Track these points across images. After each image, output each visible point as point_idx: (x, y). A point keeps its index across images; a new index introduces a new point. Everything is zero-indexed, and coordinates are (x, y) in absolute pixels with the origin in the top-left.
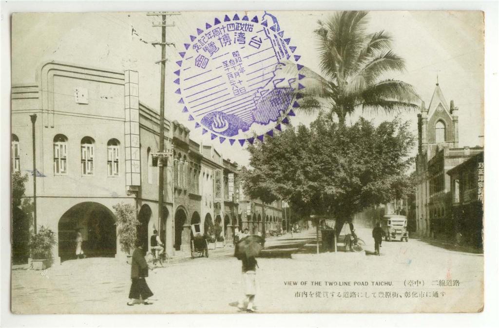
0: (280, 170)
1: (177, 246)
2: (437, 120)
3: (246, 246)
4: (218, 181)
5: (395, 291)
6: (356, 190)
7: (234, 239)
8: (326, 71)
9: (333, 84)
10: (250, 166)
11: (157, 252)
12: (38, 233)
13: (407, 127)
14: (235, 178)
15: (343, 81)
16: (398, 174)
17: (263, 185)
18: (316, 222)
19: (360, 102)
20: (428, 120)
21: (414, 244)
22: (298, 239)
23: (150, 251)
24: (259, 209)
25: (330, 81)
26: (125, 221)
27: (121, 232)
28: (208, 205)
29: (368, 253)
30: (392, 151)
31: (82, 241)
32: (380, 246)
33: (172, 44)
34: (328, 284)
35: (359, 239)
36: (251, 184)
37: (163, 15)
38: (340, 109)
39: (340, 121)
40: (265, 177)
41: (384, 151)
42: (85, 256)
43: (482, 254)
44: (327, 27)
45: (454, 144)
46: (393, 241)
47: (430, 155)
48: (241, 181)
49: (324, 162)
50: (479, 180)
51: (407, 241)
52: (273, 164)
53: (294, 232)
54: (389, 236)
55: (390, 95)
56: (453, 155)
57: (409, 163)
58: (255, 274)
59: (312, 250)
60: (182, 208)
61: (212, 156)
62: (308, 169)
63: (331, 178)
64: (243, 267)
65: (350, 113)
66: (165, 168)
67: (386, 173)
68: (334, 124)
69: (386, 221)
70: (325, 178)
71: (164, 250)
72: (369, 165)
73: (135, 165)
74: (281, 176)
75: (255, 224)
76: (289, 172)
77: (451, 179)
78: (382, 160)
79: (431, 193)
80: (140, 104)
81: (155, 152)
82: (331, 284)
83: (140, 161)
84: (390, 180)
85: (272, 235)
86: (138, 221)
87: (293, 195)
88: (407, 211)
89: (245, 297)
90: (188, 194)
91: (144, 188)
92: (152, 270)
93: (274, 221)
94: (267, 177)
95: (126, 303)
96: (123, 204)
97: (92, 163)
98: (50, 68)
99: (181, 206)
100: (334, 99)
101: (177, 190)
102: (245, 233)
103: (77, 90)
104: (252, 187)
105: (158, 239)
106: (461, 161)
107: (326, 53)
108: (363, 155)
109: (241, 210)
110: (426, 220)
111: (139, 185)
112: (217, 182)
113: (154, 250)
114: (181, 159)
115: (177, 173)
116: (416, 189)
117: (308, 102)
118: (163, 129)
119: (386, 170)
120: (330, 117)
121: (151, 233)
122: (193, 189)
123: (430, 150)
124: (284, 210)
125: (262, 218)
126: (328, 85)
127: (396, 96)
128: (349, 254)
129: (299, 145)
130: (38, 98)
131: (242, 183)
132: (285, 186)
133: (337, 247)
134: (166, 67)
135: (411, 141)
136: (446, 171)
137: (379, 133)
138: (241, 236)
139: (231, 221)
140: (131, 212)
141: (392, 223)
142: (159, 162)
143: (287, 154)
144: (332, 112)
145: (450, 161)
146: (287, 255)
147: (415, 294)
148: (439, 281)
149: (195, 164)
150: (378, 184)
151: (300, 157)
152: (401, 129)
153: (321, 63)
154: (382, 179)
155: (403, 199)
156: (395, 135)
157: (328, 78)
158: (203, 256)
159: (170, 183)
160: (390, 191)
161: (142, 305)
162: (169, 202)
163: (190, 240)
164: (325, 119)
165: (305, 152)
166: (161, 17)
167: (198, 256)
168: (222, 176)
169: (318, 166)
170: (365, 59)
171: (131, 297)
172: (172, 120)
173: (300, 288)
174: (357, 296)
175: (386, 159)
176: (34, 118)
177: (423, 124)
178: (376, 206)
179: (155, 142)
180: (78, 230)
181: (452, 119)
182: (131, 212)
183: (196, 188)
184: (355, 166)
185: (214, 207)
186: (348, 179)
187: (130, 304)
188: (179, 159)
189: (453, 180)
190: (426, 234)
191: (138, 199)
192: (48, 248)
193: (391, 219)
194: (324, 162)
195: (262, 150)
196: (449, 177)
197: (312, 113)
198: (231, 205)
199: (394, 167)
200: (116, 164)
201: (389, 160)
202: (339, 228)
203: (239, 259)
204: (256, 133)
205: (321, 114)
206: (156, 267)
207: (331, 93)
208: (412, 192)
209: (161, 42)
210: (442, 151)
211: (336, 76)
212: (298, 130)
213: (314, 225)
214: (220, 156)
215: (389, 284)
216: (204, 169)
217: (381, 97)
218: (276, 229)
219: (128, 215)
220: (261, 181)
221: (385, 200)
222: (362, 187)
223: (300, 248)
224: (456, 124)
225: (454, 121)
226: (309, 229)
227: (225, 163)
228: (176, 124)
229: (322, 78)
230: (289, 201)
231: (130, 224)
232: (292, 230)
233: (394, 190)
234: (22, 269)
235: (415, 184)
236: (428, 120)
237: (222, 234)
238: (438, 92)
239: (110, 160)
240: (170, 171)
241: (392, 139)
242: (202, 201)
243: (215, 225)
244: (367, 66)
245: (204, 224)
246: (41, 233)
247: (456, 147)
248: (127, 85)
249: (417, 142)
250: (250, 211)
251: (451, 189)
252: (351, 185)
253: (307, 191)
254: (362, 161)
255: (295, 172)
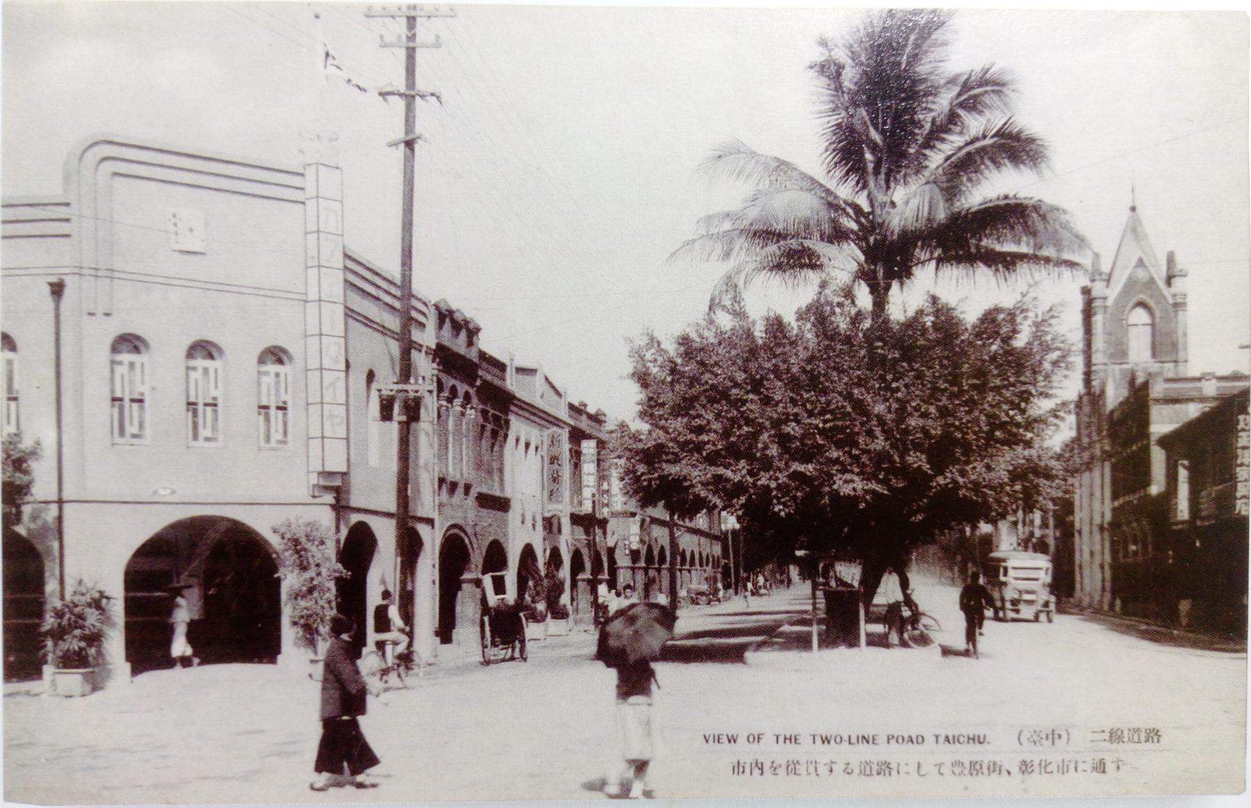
0: (715, 432)
1: (445, 631)
2: (1131, 304)
3: (629, 632)
4: (554, 460)
5: (992, 758)
6: (918, 480)
7: (596, 613)
8: (839, 173)
9: (857, 209)
10: (638, 421)
11: (389, 648)
12: (68, 597)
13: (1053, 321)
14: (599, 453)
15: (886, 199)
16: (1028, 444)
17: (673, 470)
18: (809, 570)
19: (928, 256)
20: (1110, 302)
21: (1068, 626)
22: (760, 613)
23: (370, 646)
24: (660, 535)
25: (850, 199)
26: (304, 568)
27: (297, 596)
28: (529, 523)
29: (947, 652)
30: (1013, 385)
31: (188, 621)
32: (981, 634)
33: (433, 95)
34: (818, 740)
35: (924, 614)
36: (641, 468)
37: (408, 18)
38: (875, 272)
39: (875, 304)
40: (677, 450)
41: (992, 385)
42: (196, 660)
43: (1243, 655)
44: (842, 56)
45: (1176, 366)
46: (1014, 620)
47: (1114, 395)
48: (615, 461)
49: (832, 412)
50: (1239, 462)
51: (1050, 621)
52: (699, 416)
53: (753, 594)
54: (1003, 608)
55: (1009, 236)
56: (1174, 395)
57: (1057, 417)
58: (650, 705)
59: (803, 642)
60: (456, 531)
61: (538, 395)
62: (791, 428)
63: (849, 453)
64: (618, 687)
65: (902, 284)
66: (413, 425)
67: (997, 441)
68: (860, 311)
69: (994, 569)
70: (834, 454)
71: (410, 645)
72: (950, 420)
73: (332, 417)
74: (720, 447)
75: (652, 573)
76: (739, 436)
77: (1168, 459)
78: (986, 406)
79: (1115, 497)
80: (347, 256)
81: (387, 382)
82: (826, 740)
83: (347, 404)
84: (1004, 462)
85: (694, 602)
86: (340, 566)
87: (750, 496)
88: (1051, 542)
89: (624, 765)
90: (474, 492)
91: (356, 480)
92: (377, 696)
93: (701, 565)
94: (683, 450)
95: (308, 785)
96: (301, 521)
97: (215, 411)
98: (99, 158)
99: (454, 526)
100: (861, 248)
101: (447, 485)
102: (626, 597)
103: (174, 216)
104: (643, 474)
105: (394, 613)
106: (1193, 411)
107: (839, 126)
108: (935, 391)
109: (616, 536)
110: (1102, 567)
111: (344, 469)
112: (552, 463)
113: (381, 645)
114: (457, 402)
115: (447, 439)
116: (1077, 484)
117: (790, 254)
118: (408, 322)
119: (998, 433)
120: (849, 294)
121: (373, 599)
122: (489, 481)
123: (1115, 381)
124: (726, 538)
125: (668, 559)
126: (844, 210)
127: (1024, 239)
128: (897, 653)
129: (768, 365)
130: (67, 236)
131: (617, 467)
132: (729, 474)
133: (868, 635)
134: (417, 158)
135: (1064, 356)
136: (1154, 438)
137: (978, 335)
138: (615, 603)
139: (588, 565)
140: (322, 543)
141: (1011, 573)
142: (397, 408)
143: (734, 391)
144: (854, 281)
145: (1167, 410)
146: (734, 655)
147: (1045, 767)
148: (1107, 731)
149: (493, 415)
150: (977, 470)
151: (767, 397)
152: (1037, 325)
153: (826, 150)
154: (985, 456)
155: (1042, 510)
156: (1020, 342)
157: (845, 191)
158: (512, 659)
159: (426, 465)
160: (1008, 488)
161: (350, 789)
162: (425, 515)
163: (478, 616)
164: (837, 300)
165: (780, 383)
166: (404, 21)
167: (502, 657)
168: (566, 446)
169: (815, 422)
170: (943, 140)
171: (321, 766)
172: (433, 299)
173: (745, 752)
174: (894, 773)
175: (998, 405)
176: (57, 290)
177: (1095, 314)
178: (968, 530)
179: (387, 357)
180: (178, 592)
181: (1171, 301)
182: (322, 543)
183: (496, 478)
184: (913, 422)
185: (545, 528)
186: (897, 459)
187: (317, 786)
188: (450, 400)
189: (1172, 462)
190: (1101, 602)
191: (341, 508)
192: (94, 639)
193: (1010, 564)
194: (832, 412)
195: (669, 379)
196: (1163, 452)
197: (801, 282)
198: (588, 522)
199: (1018, 425)
200: (280, 413)
201: (1005, 407)
202: (871, 583)
203: (609, 665)
204: (655, 334)
205: (823, 285)
206: (387, 690)
207: (852, 231)
208: (1066, 492)
209: (403, 89)
210: (1145, 385)
211: (865, 186)
212: (764, 329)
213: (804, 576)
214: (559, 394)
215: (978, 740)
216: (518, 427)
217: (984, 242)
218: (704, 587)
219: (314, 549)
220: (668, 461)
221: (994, 514)
222: (932, 478)
223: (769, 635)
224: (1180, 313)
225: (1176, 305)
226: (791, 587)
227: (572, 413)
228: (444, 311)
229: (828, 191)
230: (740, 513)
231: (319, 574)
232: (746, 590)
233: (1018, 487)
234: (28, 693)
235: (1074, 472)
236: (1110, 302)
237: (565, 599)
238: (1134, 230)
239: (265, 403)
240: (427, 434)
241: (1010, 352)
242: (511, 512)
243: (547, 576)
244: (947, 159)
245: (516, 571)
246: (77, 599)
247: (1182, 375)
248: (311, 205)
249: (1078, 361)
250: (638, 539)
251: (1168, 484)
252: (904, 471)
253: (787, 486)
254: (932, 409)
255: (755, 436)
